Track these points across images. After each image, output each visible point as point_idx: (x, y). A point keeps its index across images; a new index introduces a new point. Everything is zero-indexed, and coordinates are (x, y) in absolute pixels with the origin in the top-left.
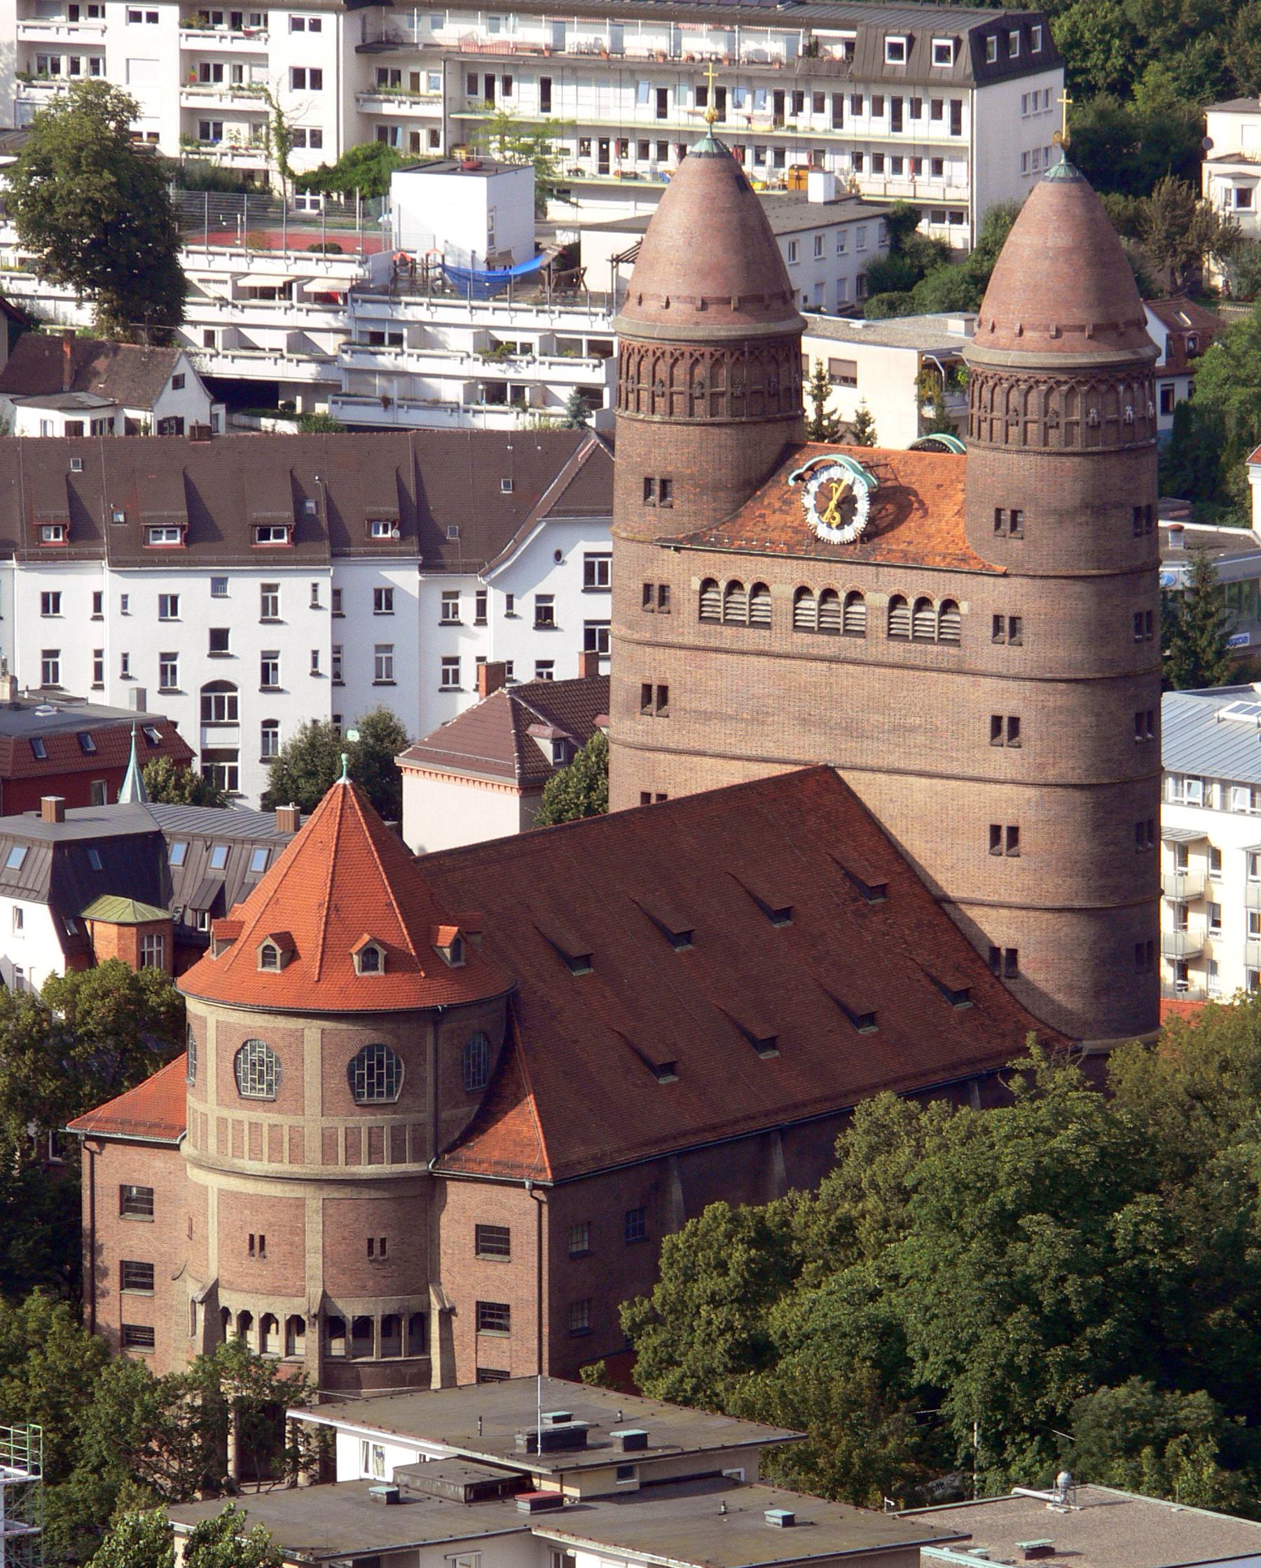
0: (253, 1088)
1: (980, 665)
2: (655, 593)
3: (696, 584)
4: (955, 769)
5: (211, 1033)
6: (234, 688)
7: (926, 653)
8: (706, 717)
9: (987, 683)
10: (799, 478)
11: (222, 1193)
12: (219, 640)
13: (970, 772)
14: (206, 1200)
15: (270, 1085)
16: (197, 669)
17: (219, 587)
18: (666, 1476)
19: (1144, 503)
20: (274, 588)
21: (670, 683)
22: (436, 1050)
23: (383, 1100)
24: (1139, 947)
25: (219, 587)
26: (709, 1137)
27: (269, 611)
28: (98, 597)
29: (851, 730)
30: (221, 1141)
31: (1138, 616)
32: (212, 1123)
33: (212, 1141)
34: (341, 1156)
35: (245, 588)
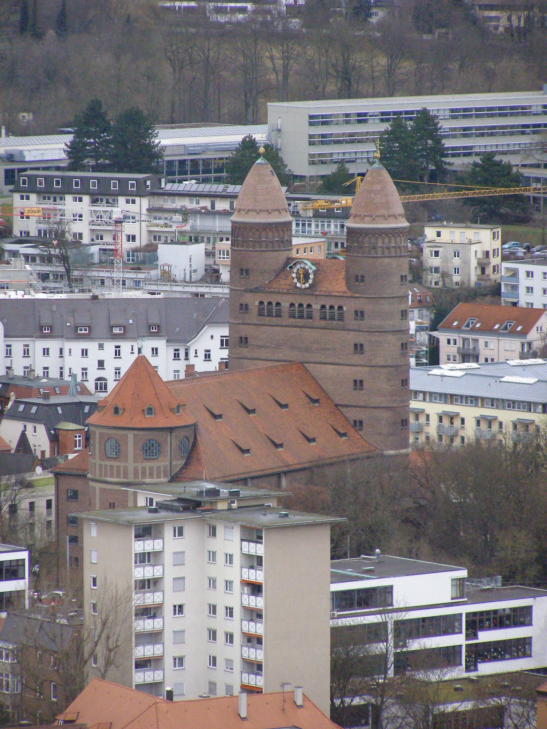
0: (111, 454)
1: (351, 327)
2: (244, 307)
3: (257, 303)
4: (341, 361)
5: (97, 436)
6: (106, 380)
7: (332, 324)
8: (259, 347)
9: (352, 333)
10: (291, 267)
11: (100, 489)
12: (101, 364)
13: (347, 363)
14: (95, 492)
15: (116, 453)
16: (94, 373)
17: (101, 347)
18: (246, 505)
19: (404, 274)
20: (119, 347)
21: (248, 336)
22: (171, 441)
23: (155, 480)
24: (402, 421)
25: (101, 347)
26: (261, 473)
27: (118, 353)
28: (61, 350)
29: (308, 350)
30: (100, 471)
31: (402, 311)
32: (98, 466)
33: (97, 472)
34: (140, 476)
35: (110, 346)
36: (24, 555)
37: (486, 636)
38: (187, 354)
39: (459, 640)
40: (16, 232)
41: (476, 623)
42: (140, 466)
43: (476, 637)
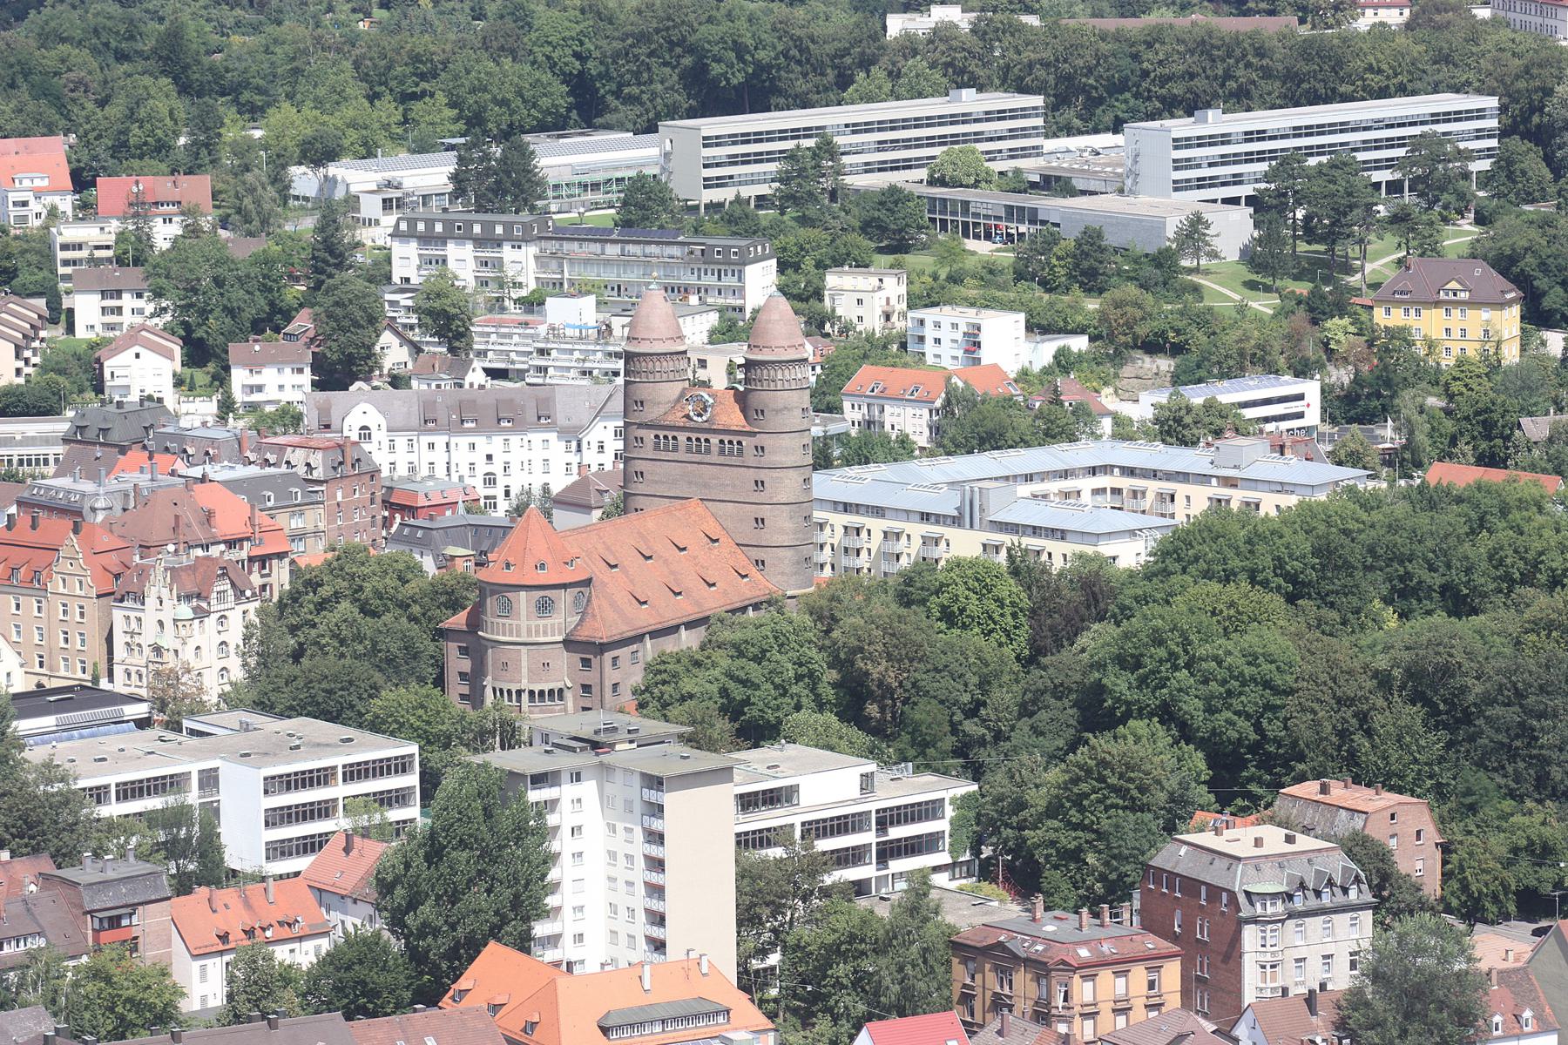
12: (489, 457)
35: (498, 440)
36: (413, 748)
37: (895, 833)
38: (579, 446)
39: (869, 837)
40: (396, 279)
41: (886, 819)
42: (533, 623)
43: (885, 833)
